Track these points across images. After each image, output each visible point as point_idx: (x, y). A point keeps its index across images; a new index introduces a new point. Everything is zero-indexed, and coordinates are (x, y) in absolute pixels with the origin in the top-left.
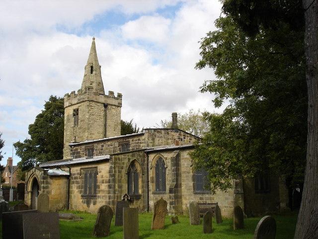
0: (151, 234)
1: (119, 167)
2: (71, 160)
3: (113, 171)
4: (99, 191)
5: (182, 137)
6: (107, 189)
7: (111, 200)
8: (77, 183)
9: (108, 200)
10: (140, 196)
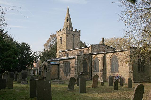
2: (60, 58)
8: (62, 67)
9: (74, 74)
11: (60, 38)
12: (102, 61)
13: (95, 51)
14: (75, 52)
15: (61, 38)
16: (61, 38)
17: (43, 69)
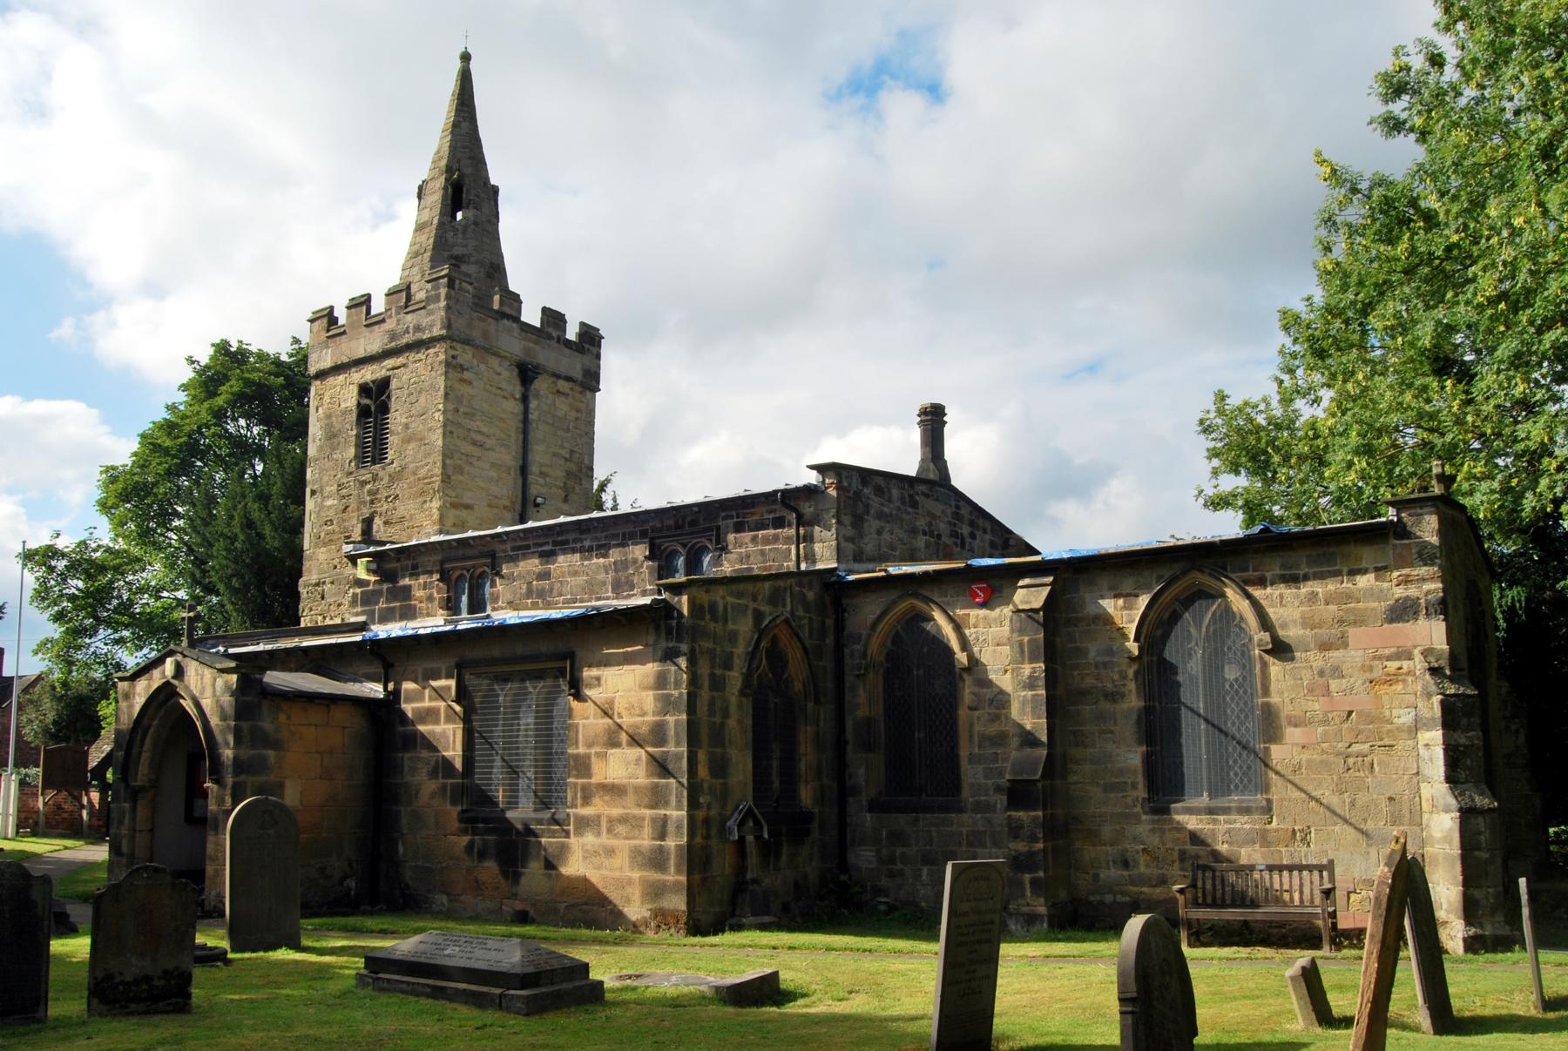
0: (339, 997)
1: (712, 654)
2: (362, 627)
5: (965, 530)
9: (646, 841)
10: (807, 817)
11: (350, 398)
12: (1027, 669)
13: (869, 546)
15: (375, 401)
16: (375, 401)
17: (145, 757)
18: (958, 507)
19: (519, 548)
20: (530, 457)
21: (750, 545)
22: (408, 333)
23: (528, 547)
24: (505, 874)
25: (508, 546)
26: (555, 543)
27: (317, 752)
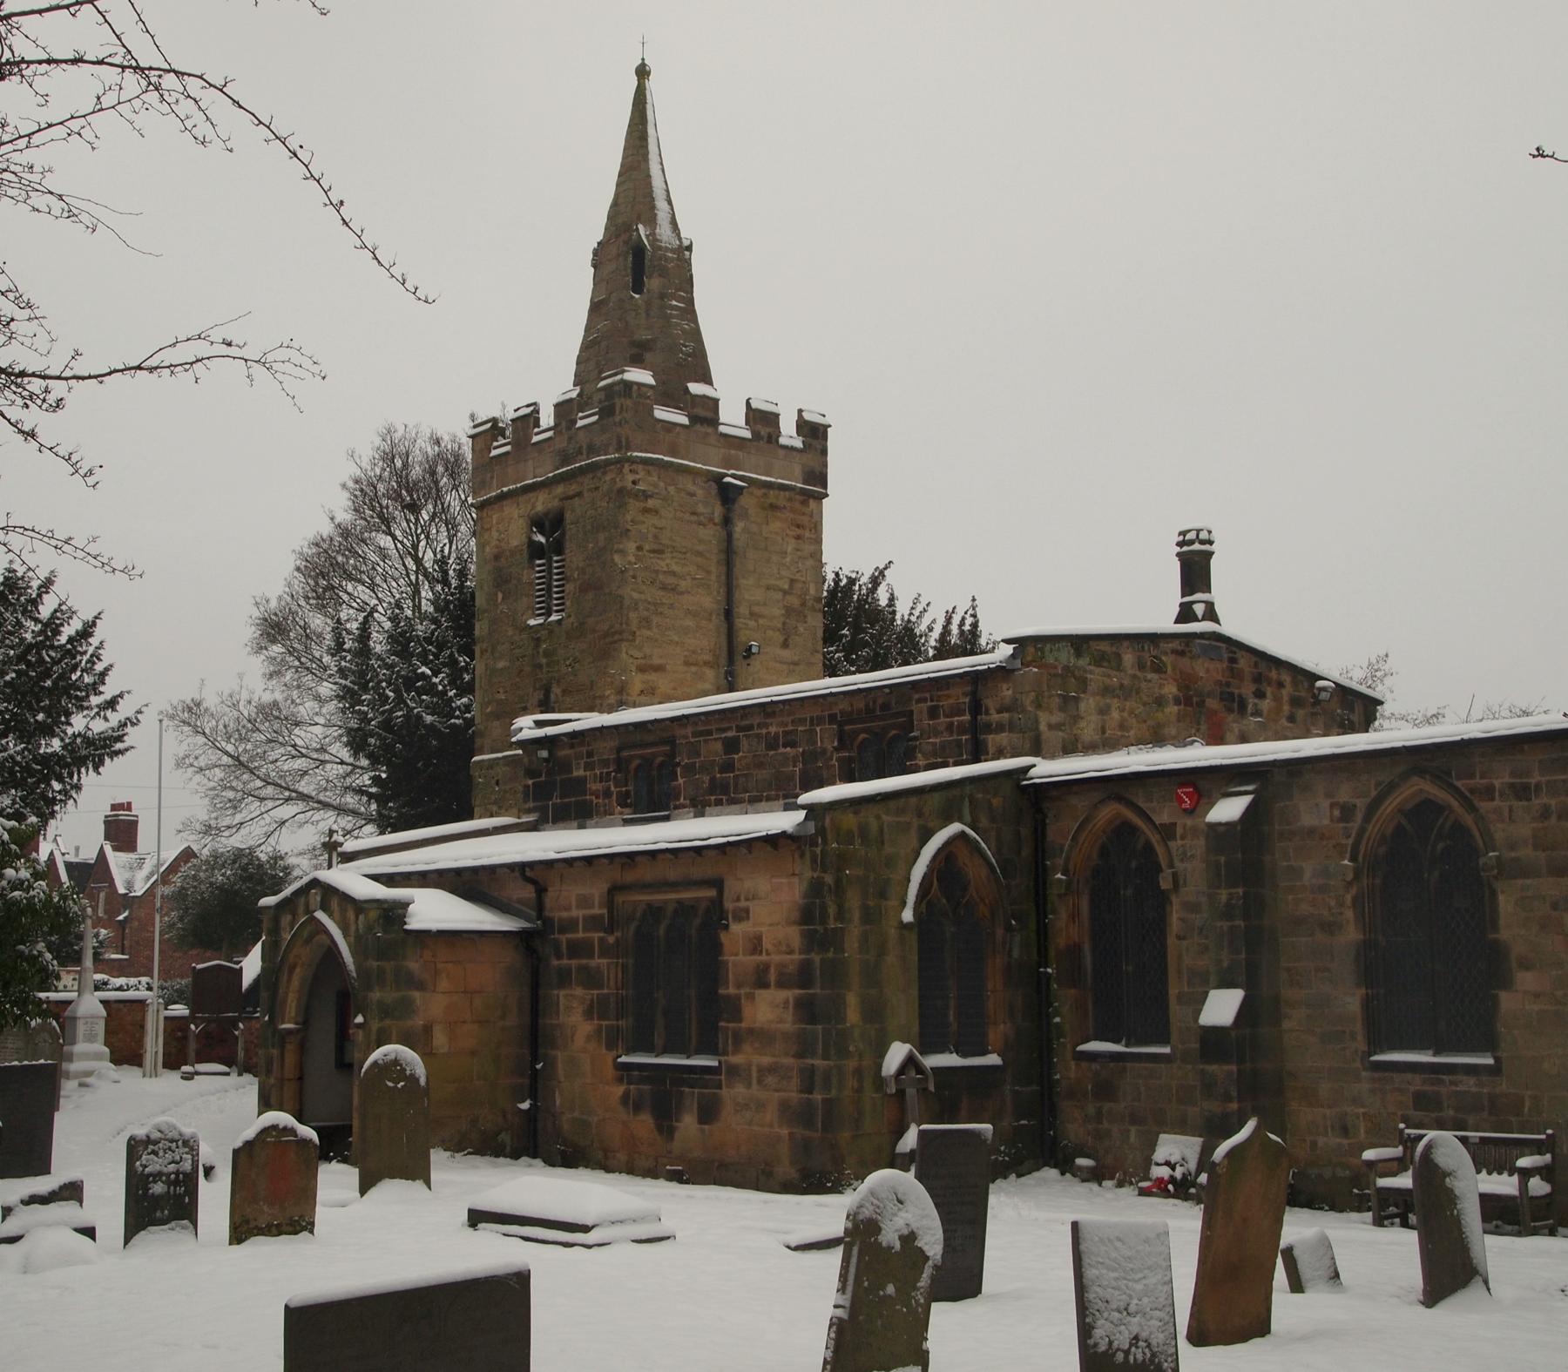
3: (832, 910)
4: (738, 1040)
6: (789, 1025)
7: (818, 1097)
8: (591, 979)
9: (794, 1096)
14: (772, 743)
18: (1233, 660)
19: (701, 734)
20: (737, 595)
21: (945, 734)
22: (582, 454)
23: (709, 733)
24: (660, 1129)
25: (689, 730)
26: (739, 729)
27: (465, 992)
